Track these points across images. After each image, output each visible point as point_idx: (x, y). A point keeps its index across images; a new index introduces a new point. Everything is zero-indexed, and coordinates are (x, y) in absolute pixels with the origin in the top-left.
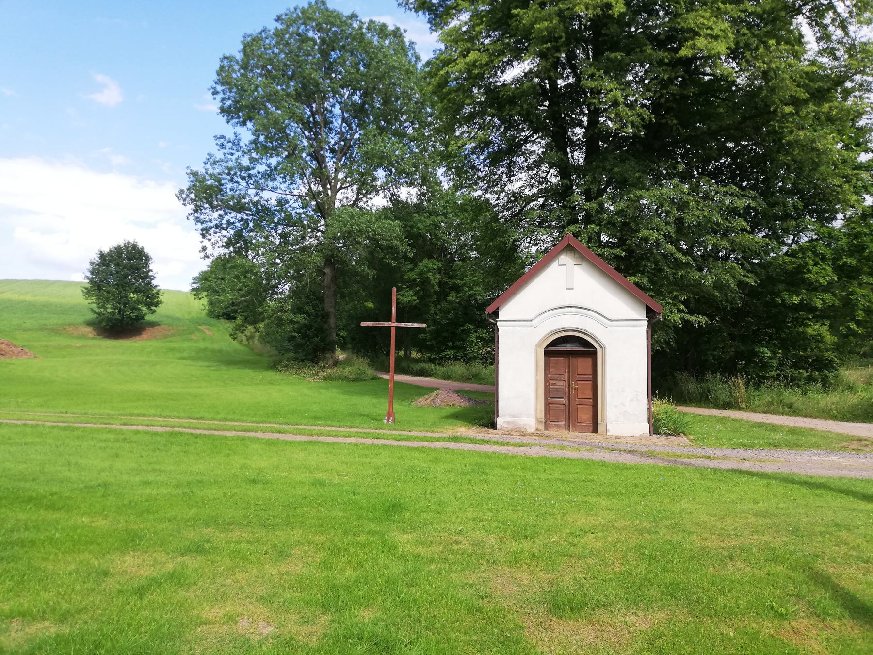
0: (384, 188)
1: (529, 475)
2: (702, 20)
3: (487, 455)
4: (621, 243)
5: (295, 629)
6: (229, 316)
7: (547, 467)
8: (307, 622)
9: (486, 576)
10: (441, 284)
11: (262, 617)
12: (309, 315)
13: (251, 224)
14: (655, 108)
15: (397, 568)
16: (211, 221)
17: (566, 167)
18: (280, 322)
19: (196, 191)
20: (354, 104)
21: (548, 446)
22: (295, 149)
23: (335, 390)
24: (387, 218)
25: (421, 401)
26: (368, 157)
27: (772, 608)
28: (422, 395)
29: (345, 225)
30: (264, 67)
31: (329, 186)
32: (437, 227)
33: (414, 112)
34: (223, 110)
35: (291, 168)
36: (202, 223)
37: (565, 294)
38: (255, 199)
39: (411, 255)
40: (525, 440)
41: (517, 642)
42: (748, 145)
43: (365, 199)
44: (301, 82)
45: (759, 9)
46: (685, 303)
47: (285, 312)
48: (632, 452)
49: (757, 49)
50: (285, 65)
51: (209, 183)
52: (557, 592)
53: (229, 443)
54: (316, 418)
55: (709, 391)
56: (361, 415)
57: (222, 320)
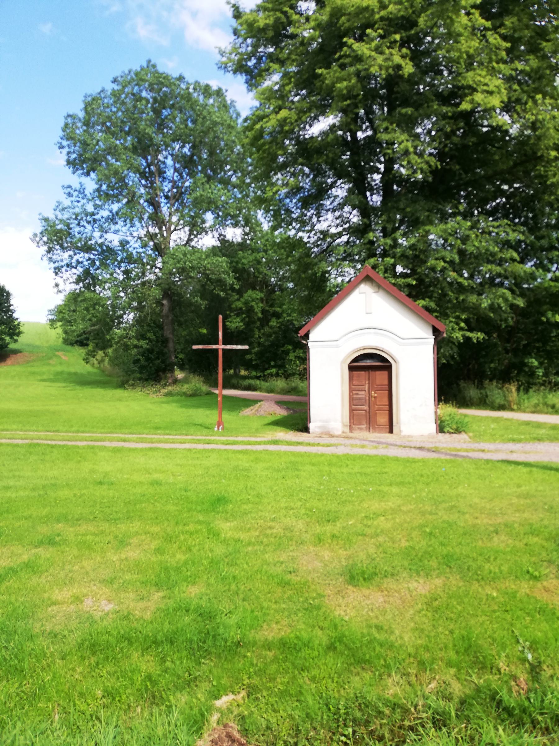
0: (212, 229)
1: (333, 470)
2: (479, 78)
3: (300, 455)
4: (414, 272)
5: (132, 605)
6: (82, 343)
7: (349, 463)
8: (142, 599)
9: (295, 554)
10: (263, 311)
11: (104, 596)
12: (150, 340)
13: (97, 263)
14: (441, 155)
15: (220, 550)
16: (62, 261)
17: (366, 209)
18: (126, 348)
19: (48, 234)
20: (184, 156)
21: (352, 445)
22: (134, 196)
23: (174, 404)
24: (215, 255)
25: (247, 412)
26: (197, 202)
27: (528, 572)
28: (247, 406)
29: (179, 262)
30: (104, 124)
31: (164, 228)
32: (259, 262)
33: (236, 162)
34: (69, 163)
35: (131, 213)
36: (55, 263)
37: (366, 319)
38: (100, 241)
39: (237, 287)
40: (333, 441)
41: (319, 608)
42: (519, 188)
43: (196, 240)
44: (137, 137)
45: (527, 68)
46: (466, 321)
47: (130, 338)
48: (421, 448)
49: (526, 103)
50: (123, 122)
51: (59, 227)
52: (352, 565)
53: (81, 451)
54: (157, 428)
55: (487, 396)
56: (195, 425)
57: (76, 347)
